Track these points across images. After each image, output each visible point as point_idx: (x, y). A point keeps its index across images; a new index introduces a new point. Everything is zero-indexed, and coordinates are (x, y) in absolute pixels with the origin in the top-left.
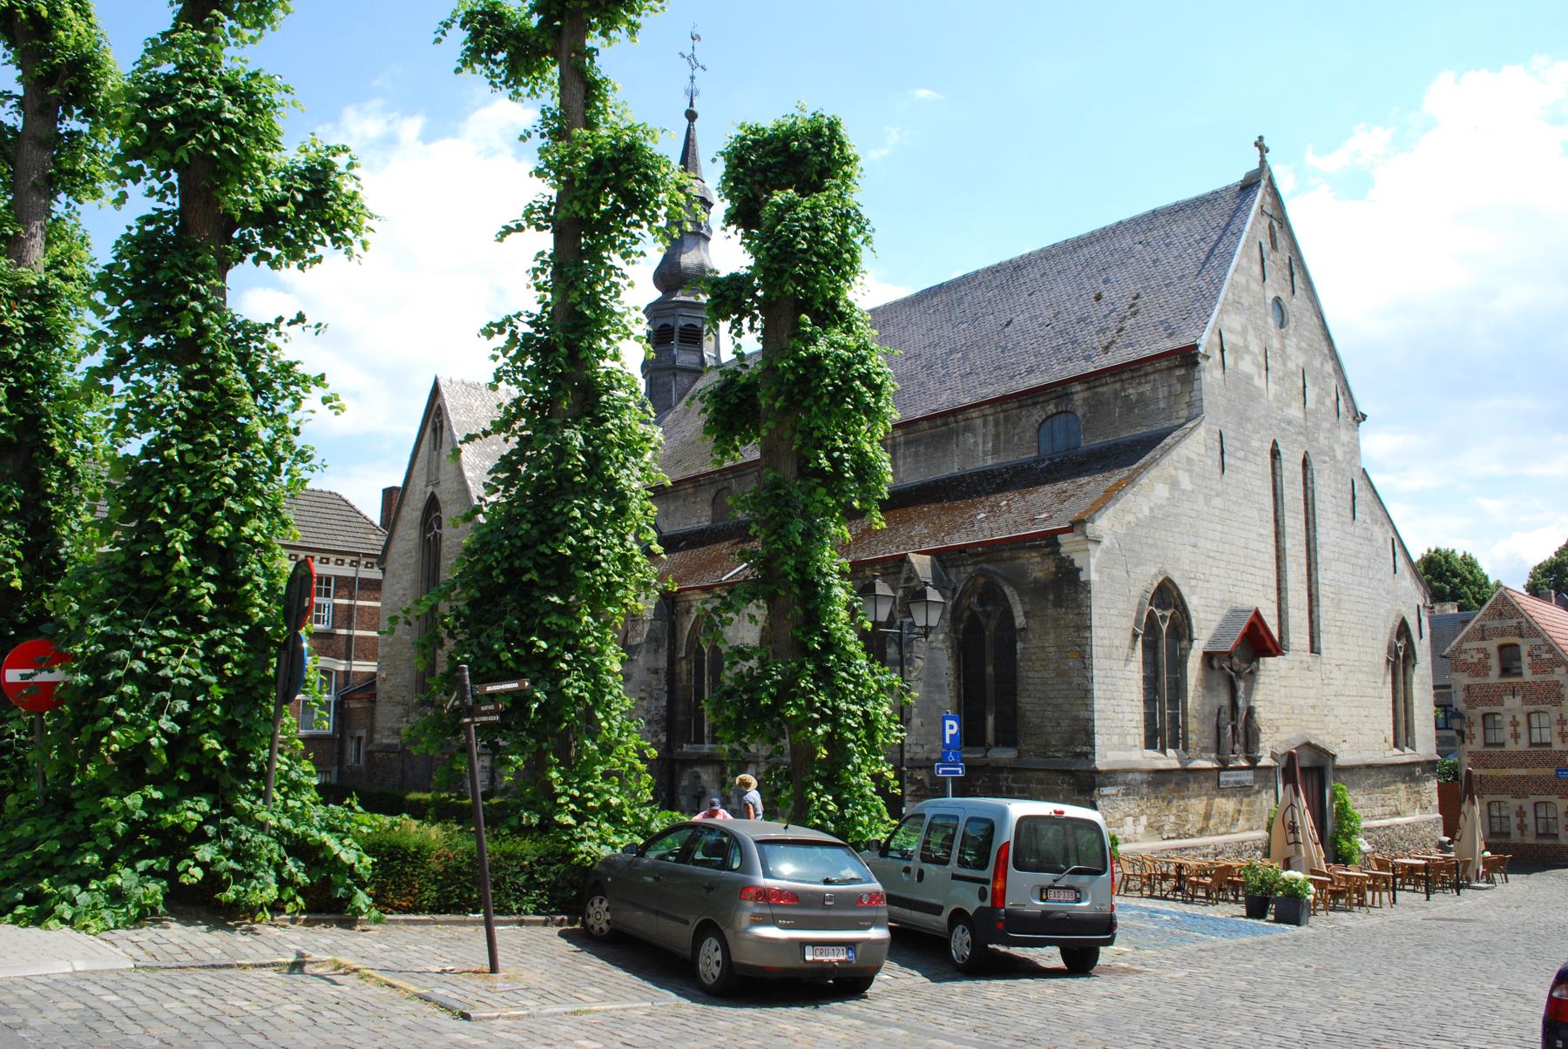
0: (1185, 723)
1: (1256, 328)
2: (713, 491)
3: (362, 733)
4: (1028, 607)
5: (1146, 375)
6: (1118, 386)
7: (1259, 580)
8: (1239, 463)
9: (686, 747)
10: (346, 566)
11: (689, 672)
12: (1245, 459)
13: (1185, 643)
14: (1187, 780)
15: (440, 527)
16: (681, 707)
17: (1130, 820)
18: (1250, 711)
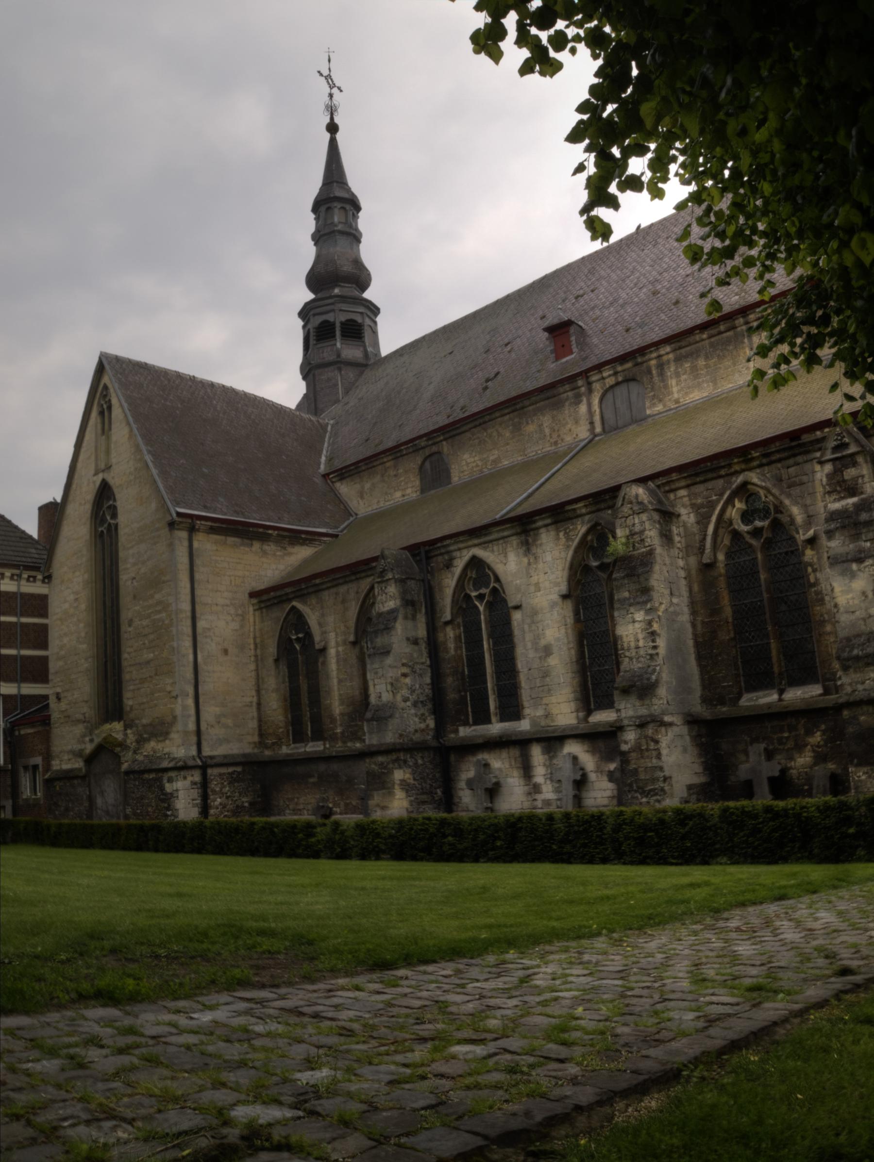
3: (38, 760)
9: (464, 732)
10: (39, 583)
11: (458, 638)
15: (114, 515)
16: (450, 681)
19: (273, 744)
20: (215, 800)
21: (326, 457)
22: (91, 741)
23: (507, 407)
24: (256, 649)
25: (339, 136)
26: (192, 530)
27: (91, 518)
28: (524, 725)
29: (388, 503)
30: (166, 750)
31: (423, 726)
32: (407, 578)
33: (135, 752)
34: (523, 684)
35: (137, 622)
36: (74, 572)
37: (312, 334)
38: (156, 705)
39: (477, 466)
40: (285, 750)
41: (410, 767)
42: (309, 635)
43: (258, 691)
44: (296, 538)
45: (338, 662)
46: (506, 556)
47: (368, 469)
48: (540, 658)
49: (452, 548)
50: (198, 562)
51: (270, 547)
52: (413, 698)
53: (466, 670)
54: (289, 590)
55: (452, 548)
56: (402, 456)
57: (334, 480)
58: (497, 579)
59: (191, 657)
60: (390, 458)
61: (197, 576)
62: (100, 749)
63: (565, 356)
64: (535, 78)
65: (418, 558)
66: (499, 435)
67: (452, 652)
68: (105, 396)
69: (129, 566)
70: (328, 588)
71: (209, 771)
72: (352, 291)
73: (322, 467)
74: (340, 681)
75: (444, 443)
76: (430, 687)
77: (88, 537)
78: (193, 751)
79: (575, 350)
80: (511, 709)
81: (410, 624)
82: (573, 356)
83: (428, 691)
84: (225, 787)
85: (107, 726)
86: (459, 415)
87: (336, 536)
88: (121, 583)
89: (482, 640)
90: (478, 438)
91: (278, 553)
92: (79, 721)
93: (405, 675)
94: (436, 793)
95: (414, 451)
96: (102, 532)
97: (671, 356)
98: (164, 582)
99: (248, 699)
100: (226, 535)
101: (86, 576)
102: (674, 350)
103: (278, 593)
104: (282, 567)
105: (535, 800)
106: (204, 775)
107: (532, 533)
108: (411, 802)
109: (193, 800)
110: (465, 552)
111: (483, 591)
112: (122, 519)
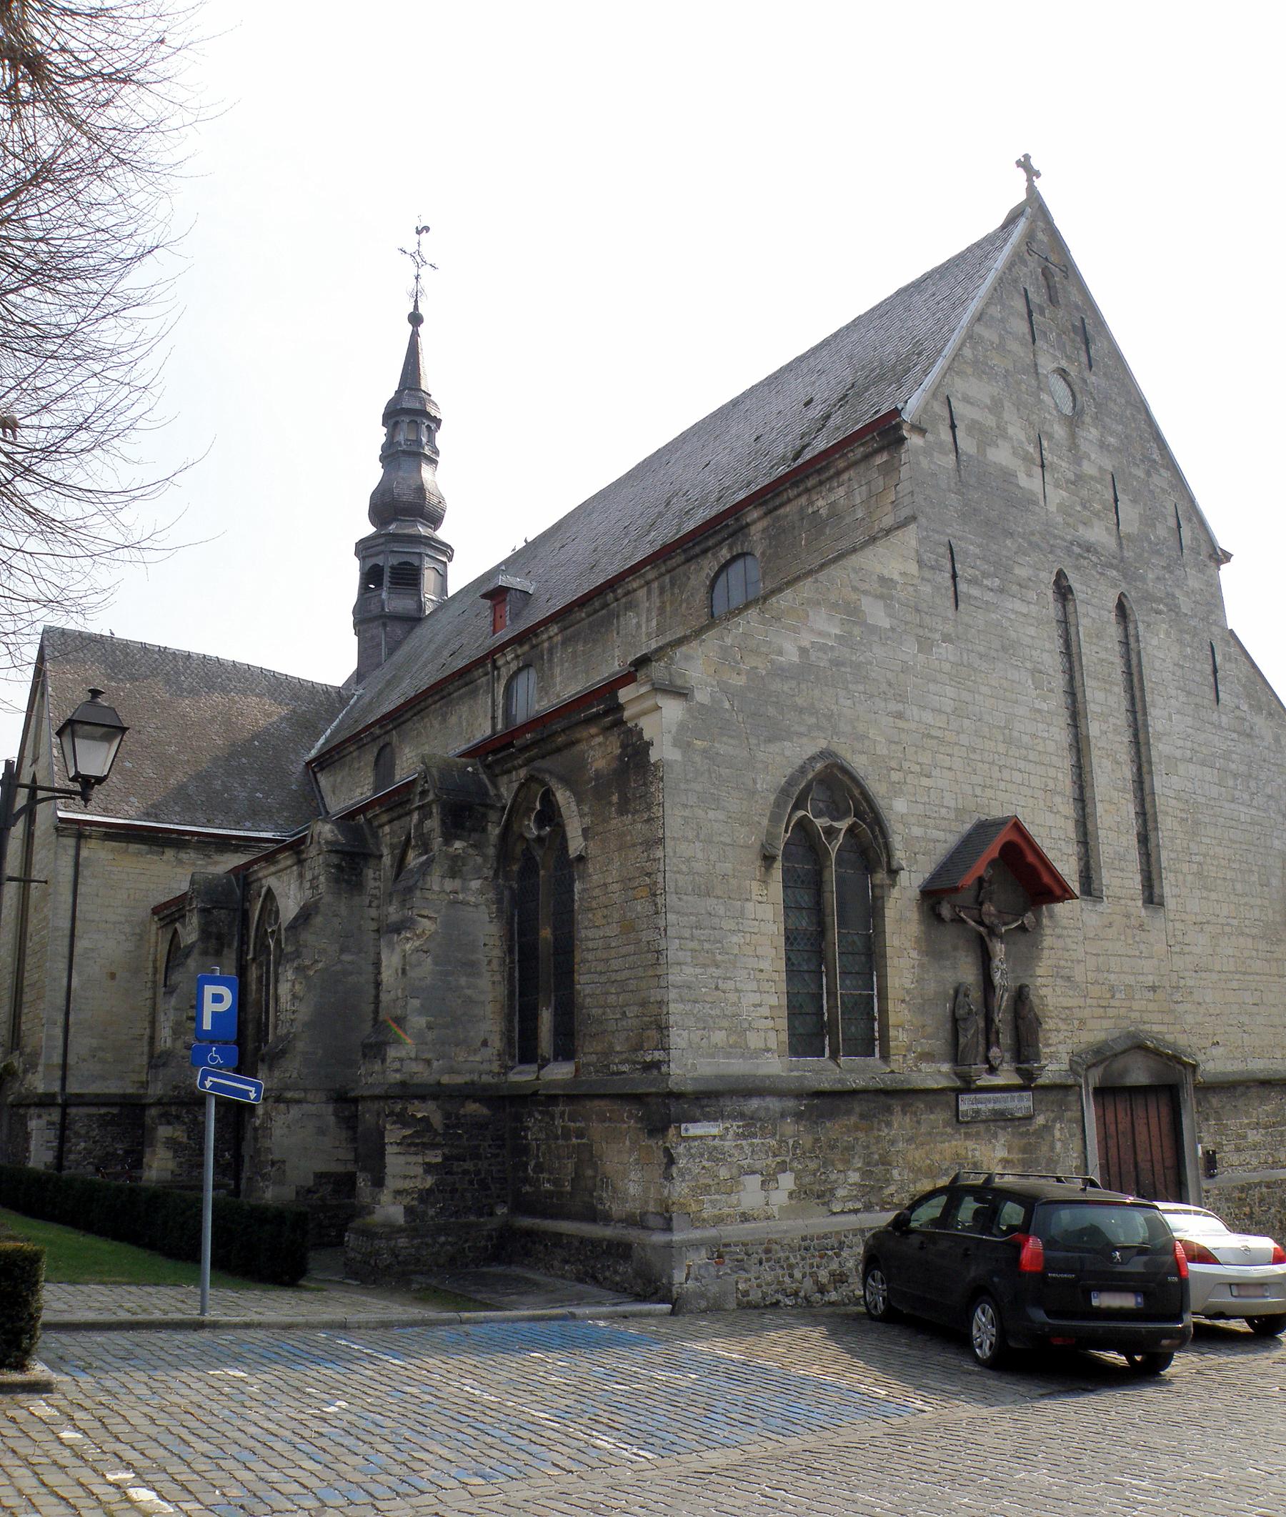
0: (884, 1011)
1: (1018, 405)
2: (376, 751)
4: (587, 820)
5: (839, 473)
6: (803, 500)
7: (1035, 782)
8: (989, 596)
12: (1001, 591)
13: (881, 877)
14: (889, 1110)
17: (754, 1181)
18: (1021, 996)
24: (155, 974)
25: (422, 329)
41: (185, 1124)
49: (260, 875)
50: (85, 872)
55: (260, 875)
59: (65, 981)
61: (82, 889)
64: (1020, 157)
72: (423, 530)
78: (56, 1088)
97: (559, 638)
102: (561, 631)
106: (64, 1115)
108: (180, 1165)
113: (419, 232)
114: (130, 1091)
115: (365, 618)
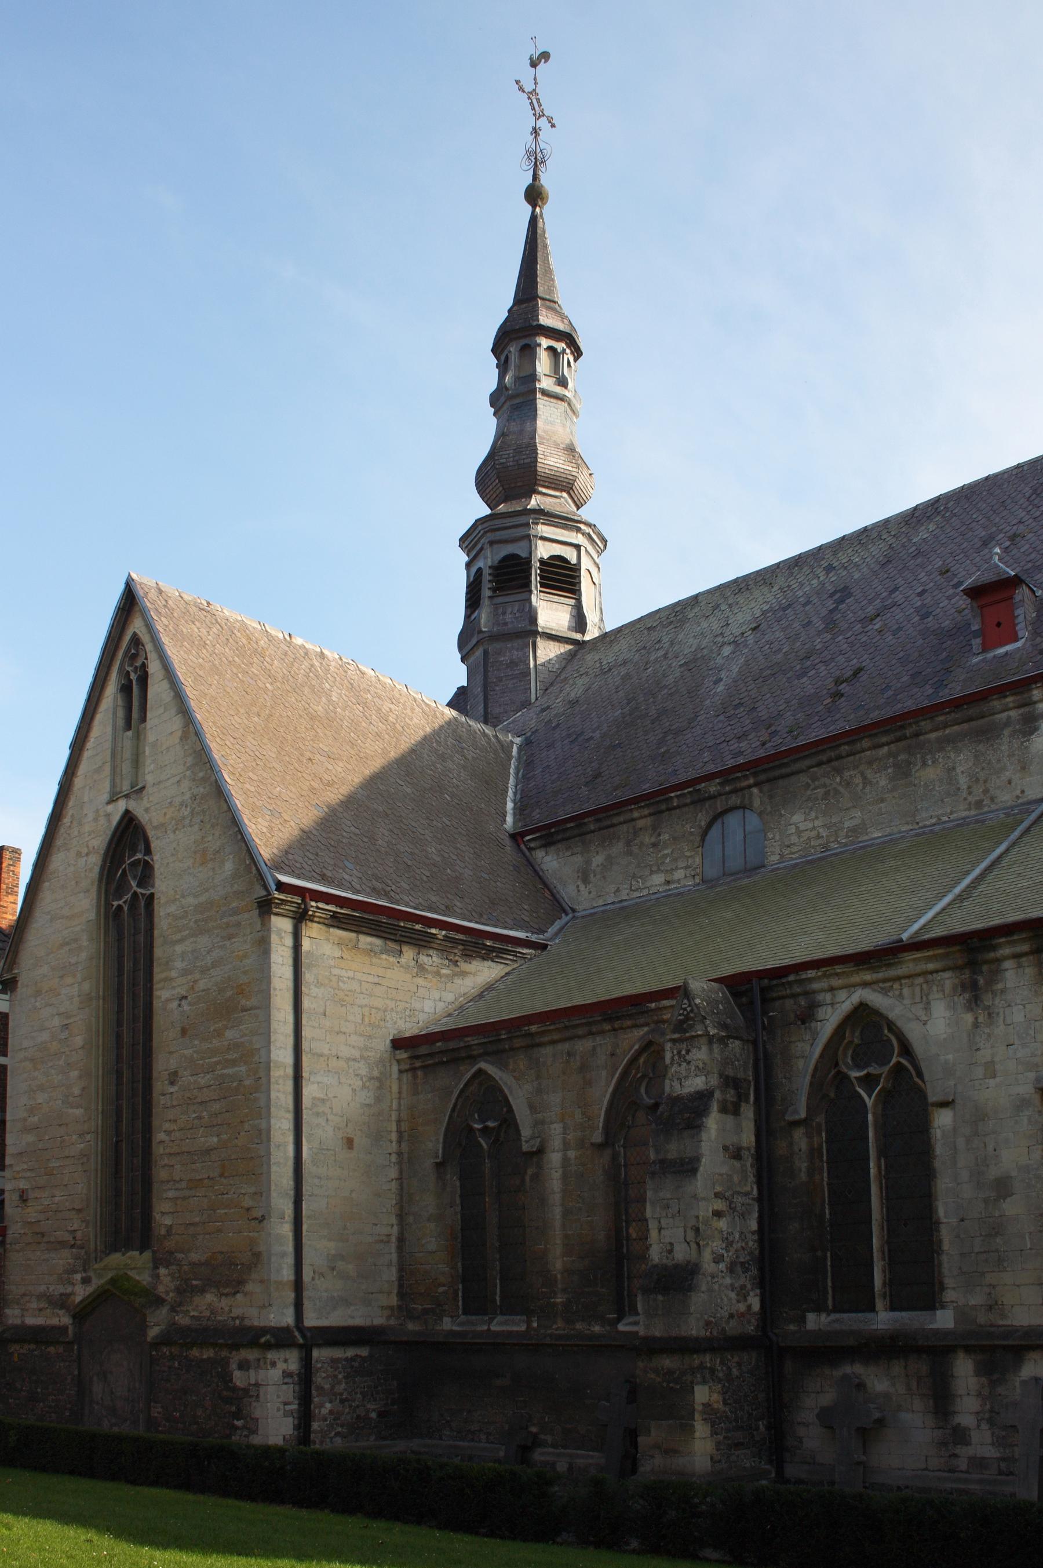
2: (703, 819)
9: (814, 1321)
11: (814, 1153)
19: (426, 1311)
20: (322, 1406)
21: (514, 801)
22: (86, 1281)
23: (886, 732)
24: (399, 1142)
25: (548, 213)
26: (300, 917)
27: (100, 881)
28: (944, 1320)
29: (636, 894)
30: (236, 1312)
31: (742, 1307)
32: (729, 1037)
33: (173, 1309)
34: (946, 1246)
35: (186, 1078)
36: (62, 977)
37: (486, 577)
38: (219, 1231)
39: (819, 837)
40: (447, 1324)
41: (720, 1381)
42: (509, 1121)
43: (401, 1217)
44: (475, 945)
45: (565, 1177)
46: (927, 1008)
47: (600, 829)
48: (986, 1201)
49: (816, 986)
50: (308, 977)
51: (431, 959)
52: (729, 1256)
53: (827, 1211)
54: (473, 1040)
55: (816, 986)
56: (669, 810)
57: (532, 845)
58: (906, 1050)
59: (291, 1149)
60: (646, 812)
61: (306, 1003)
62: (100, 1298)
63: (1002, 644)
65: (744, 1000)
66: (866, 781)
67: (803, 1176)
68: (134, 657)
69: (174, 974)
70: (553, 1042)
71: (316, 1353)
73: (509, 819)
74: (566, 1213)
75: (755, 790)
76: (755, 1237)
77: (92, 915)
78: (288, 1319)
79: (1024, 632)
80: (919, 1287)
81: (730, 1119)
82: (1019, 644)
83: (752, 1244)
84: (339, 1383)
85: (116, 1259)
86: (784, 742)
87: (544, 947)
88: (157, 1004)
89: (867, 1159)
90: (825, 786)
91: (444, 971)
92: (63, 1244)
93: (718, 1214)
94: (757, 1429)
95: (692, 803)
96: (120, 907)
98: (245, 1010)
99: (385, 1230)
100: (358, 932)
101: (86, 986)
103: (452, 1045)
104: (450, 997)
105: (955, 1456)
106: (307, 1362)
107: (985, 968)
108: (718, 1444)
109: (286, 1404)
110: (842, 995)
111: (874, 1070)
112: (163, 886)
113: (534, 64)
114: (379, 1321)
115: (469, 642)
